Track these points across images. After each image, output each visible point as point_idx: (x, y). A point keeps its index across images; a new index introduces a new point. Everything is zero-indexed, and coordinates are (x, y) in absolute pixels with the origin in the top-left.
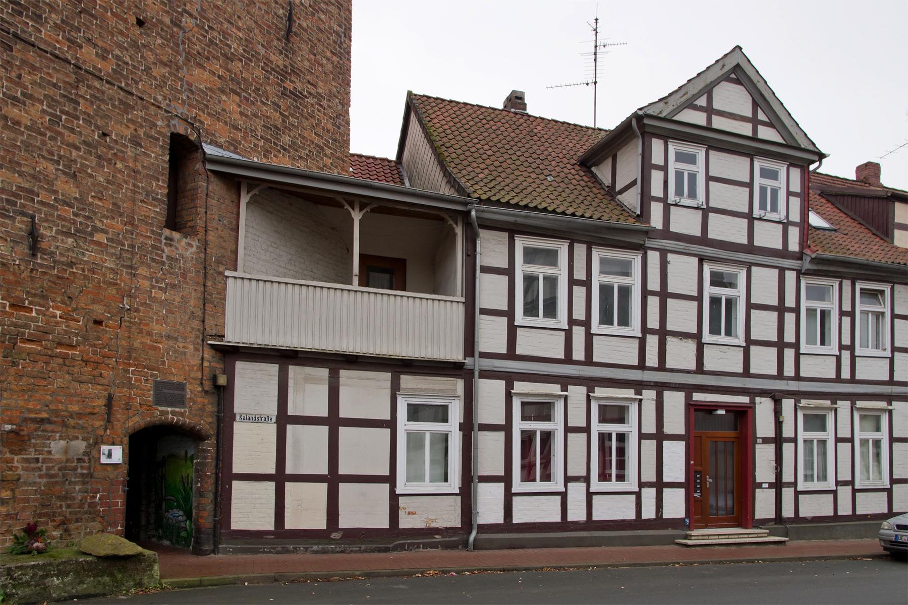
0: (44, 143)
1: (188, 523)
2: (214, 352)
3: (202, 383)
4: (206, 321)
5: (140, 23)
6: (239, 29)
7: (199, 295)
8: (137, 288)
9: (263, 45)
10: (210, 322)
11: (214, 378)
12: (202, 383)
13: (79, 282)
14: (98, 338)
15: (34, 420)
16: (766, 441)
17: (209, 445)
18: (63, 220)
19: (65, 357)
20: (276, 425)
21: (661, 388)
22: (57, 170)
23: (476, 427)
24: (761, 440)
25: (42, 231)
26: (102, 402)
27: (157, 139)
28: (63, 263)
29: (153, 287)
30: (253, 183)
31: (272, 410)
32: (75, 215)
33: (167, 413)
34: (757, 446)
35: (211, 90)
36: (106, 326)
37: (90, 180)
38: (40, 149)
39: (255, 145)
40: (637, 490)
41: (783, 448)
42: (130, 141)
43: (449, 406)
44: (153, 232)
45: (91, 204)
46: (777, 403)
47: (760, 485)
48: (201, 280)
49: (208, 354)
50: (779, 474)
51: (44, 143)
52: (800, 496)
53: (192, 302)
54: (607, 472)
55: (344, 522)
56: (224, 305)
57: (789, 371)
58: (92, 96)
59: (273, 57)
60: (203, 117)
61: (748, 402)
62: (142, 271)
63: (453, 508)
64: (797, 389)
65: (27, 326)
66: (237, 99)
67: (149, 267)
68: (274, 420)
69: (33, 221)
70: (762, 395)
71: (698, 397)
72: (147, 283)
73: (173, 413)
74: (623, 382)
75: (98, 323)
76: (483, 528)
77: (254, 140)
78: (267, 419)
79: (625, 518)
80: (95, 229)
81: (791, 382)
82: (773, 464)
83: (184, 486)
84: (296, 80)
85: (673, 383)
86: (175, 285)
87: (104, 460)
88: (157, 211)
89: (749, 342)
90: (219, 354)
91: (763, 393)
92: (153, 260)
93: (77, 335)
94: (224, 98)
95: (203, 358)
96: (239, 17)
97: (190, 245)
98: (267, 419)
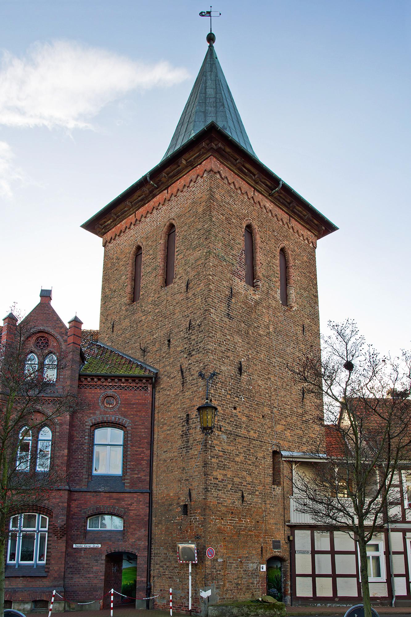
1: (279, 594)
6: (288, 405)
9: (296, 408)
10: (286, 516)
11: (289, 537)
17: (288, 563)
18: (249, 490)
20: (311, 555)
22: (247, 474)
23: (391, 553)
27: (269, 455)
29: (270, 507)
30: (296, 462)
31: (310, 549)
32: (251, 487)
36: (260, 523)
38: (243, 468)
39: (296, 446)
42: (262, 458)
43: (379, 545)
48: (283, 501)
49: (286, 528)
55: (340, 594)
58: (253, 446)
59: (299, 411)
60: (281, 442)
62: (268, 502)
63: (384, 588)
65: (242, 526)
66: (289, 431)
68: (310, 553)
69: (242, 492)
73: (278, 552)
76: (398, 597)
77: (295, 444)
78: (308, 552)
83: (276, 579)
84: (306, 416)
88: (269, 480)
90: (289, 528)
93: (253, 527)
94: (286, 432)
96: (288, 401)
98: (308, 552)
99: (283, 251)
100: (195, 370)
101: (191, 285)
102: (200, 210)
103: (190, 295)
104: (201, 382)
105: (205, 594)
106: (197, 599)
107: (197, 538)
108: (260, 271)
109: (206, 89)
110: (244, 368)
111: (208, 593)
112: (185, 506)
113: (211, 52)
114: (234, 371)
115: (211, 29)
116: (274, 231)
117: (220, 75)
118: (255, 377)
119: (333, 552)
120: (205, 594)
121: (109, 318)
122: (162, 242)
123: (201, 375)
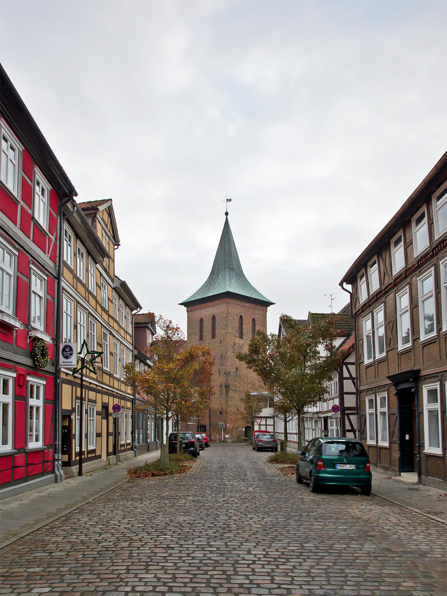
99: (254, 319)
100: (223, 371)
101: (221, 342)
102: (224, 316)
103: (221, 345)
104: (225, 375)
105: (227, 436)
106: (224, 438)
107: (225, 421)
108: (245, 332)
109: (225, 246)
110: (238, 368)
111: (228, 436)
112: (221, 412)
113: (227, 223)
114: (235, 370)
115: (229, 571)
116: (250, 314)
117: (231, 237)
118: (242, 370)
119: (266, 425)
120: (227, 436)
121: (191, 343)
122: (211, 321)
123: (225, 373)
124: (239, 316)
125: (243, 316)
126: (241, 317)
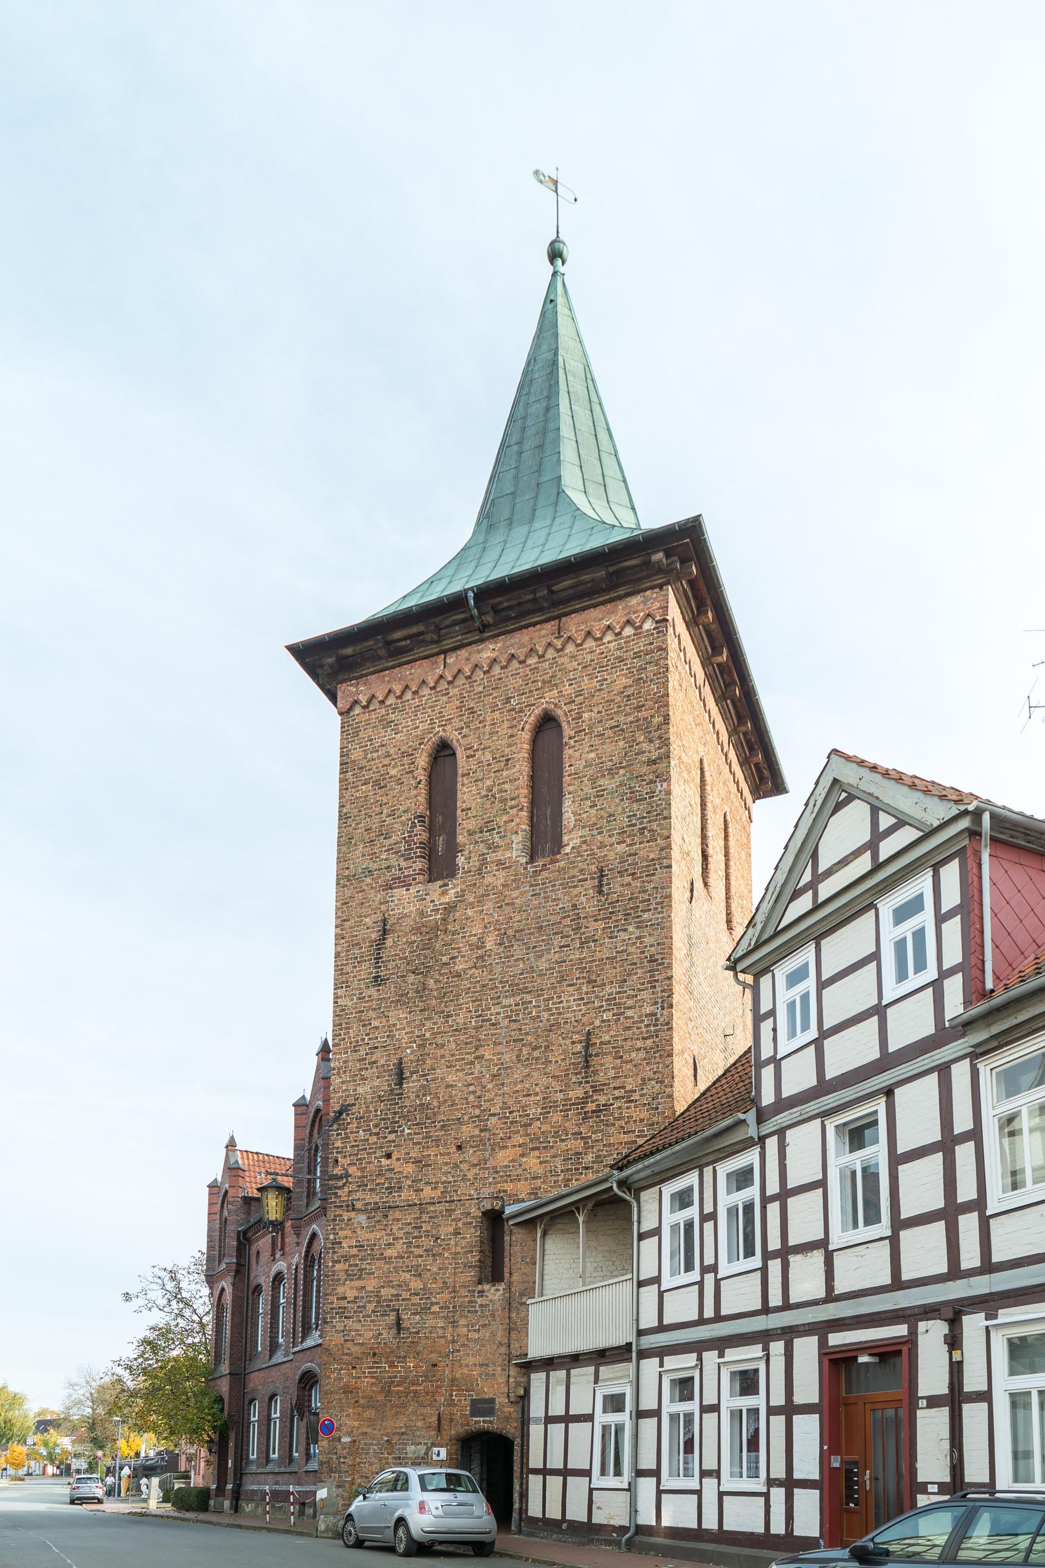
0: (404, 1262)
2: (519, 1369)
3: (508, 1396)
4: (512, 1346)
5: (459, 1148)
7: (505, 1326)
8: (458, 1335)
10: (515, 1345)
12: (508, 1396)
13: (423, 1342)
14: (434, 1376)
15: (398, 1433)
16: (934, 1402)
19: (416, 1392)
21: (789, 1334)
24: (925, 1401)
25: (403, 1317)
26: (435, 1418)
28: (414, 1333)
29: (469, 1331)
32: (420, 1299)
33: (479, 1422)
34: (919, 1413)
35: (513, 1161)
37: (429, 1273)
38: (402, 1267)
40: (764, 1490)
41: (965, 1414)
44: (469, 1291)
45: (430, 1288)
46: (955, 1322)
47: (923, 1488)
50: (957, 1467)
51: (404, 1262)
52: (663, 1496)
53: (499, 1334)
54: (690, 1466)
56: (527, 1328)
57: (970, 1258)
61: (905, 1333)
64: (987, 1291)
65: (396, 1377)
67: (466, 1317)
70: (929, 1315)
71: (836, 1339)
72: (465, 1329)
73: (484, 1422)
74: (750, 1336)
75: (434, 1365)
79: (754, 1531)
80: (432, 1304)
81: (974, 1280)
82: (946, 1445)
85: (800, 1325)
86: (486, 1325)
87: (435, 1458)
89: (899, 1224)
91: (929, 1312)
92: (469, 1311)
93: (421, 1376)
95: (509, 1376)
97: (497, 1290)
124: (531, 719)
125: (452, 735)
126: (443, 751)
